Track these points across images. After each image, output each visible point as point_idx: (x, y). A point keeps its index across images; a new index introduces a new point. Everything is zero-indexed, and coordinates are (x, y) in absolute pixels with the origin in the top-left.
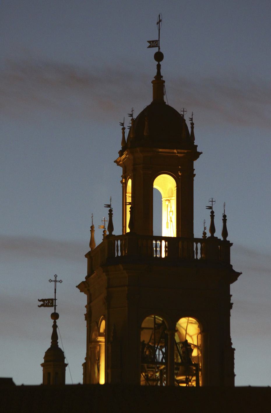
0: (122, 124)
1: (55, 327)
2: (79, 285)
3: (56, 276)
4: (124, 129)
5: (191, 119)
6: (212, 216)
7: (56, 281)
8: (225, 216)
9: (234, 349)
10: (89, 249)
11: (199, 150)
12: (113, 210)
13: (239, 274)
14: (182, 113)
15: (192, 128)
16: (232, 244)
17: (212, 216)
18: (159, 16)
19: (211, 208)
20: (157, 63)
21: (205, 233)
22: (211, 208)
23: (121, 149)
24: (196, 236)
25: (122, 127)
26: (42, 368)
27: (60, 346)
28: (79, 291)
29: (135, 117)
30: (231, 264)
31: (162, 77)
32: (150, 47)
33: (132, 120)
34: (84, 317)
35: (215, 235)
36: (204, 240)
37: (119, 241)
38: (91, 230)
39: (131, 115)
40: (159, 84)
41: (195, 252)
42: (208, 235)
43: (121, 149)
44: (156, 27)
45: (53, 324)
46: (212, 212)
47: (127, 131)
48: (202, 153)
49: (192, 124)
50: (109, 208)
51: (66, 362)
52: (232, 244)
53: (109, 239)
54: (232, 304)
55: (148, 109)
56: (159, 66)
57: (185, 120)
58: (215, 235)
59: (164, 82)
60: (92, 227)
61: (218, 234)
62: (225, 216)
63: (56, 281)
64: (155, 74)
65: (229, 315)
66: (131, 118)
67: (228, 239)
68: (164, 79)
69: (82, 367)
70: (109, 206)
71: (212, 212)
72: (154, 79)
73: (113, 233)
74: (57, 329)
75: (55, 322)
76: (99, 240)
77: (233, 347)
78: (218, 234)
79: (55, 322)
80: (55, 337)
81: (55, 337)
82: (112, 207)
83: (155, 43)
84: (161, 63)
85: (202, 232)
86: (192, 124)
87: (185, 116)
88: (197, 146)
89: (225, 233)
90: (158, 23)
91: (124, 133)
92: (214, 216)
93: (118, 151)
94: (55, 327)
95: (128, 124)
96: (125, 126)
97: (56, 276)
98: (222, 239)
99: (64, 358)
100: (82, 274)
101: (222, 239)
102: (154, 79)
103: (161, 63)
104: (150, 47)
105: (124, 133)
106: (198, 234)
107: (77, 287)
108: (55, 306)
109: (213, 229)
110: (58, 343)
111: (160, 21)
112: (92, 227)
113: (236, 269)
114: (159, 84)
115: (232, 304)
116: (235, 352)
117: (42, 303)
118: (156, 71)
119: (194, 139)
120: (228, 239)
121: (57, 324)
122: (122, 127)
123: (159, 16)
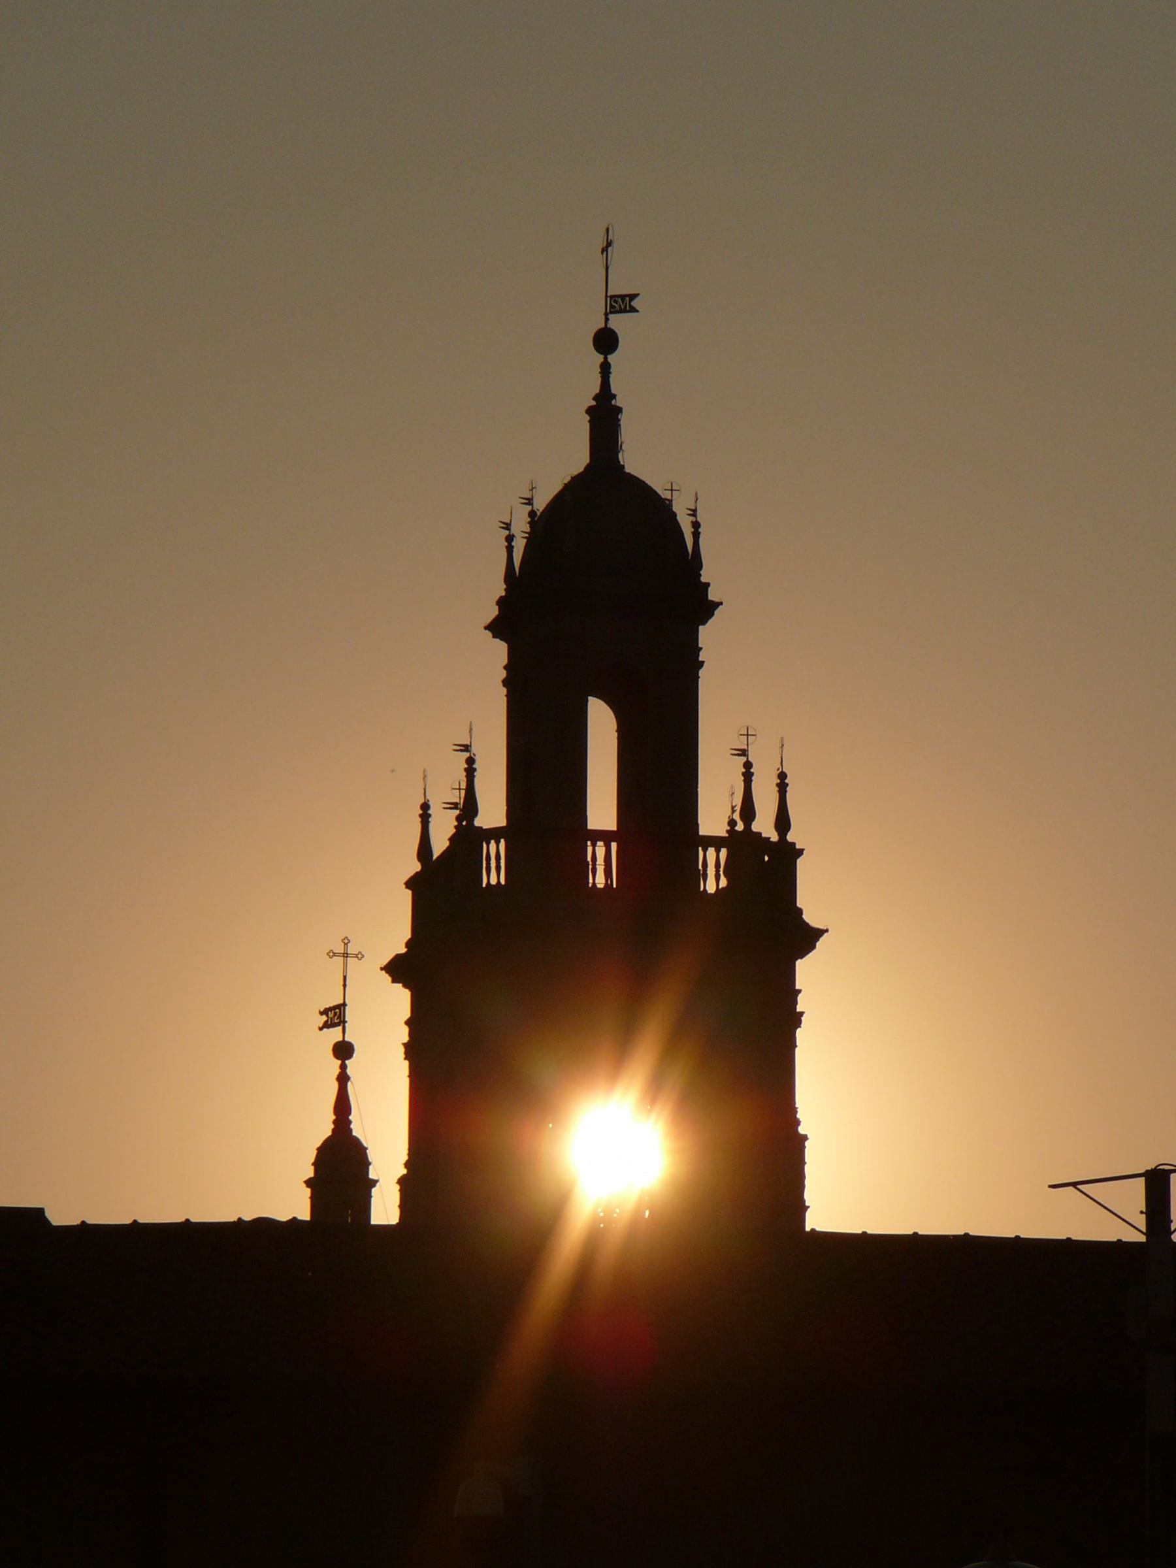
0: (507, 526)
1: (343, 1079)
2: (389, 963)
3: (346, 942)
4: (510, 539)
5: (694, 513)
6: (748, 776)
7: (346, 955)
8: (782, 776)
9: (805, 1138)
10: (417, 867)
11: (713, 595)
12: (477, 758)
13: (820, 933)
14: (666, 495)
15: (696, 535)
16: (801, 852)
17: (748, 776)
18: (608, 230)
19: (744, 753)
20: (601, 358)
21: (732, 823)
22: (744, 753)
23: (503, 594)
24: (591, 825)
25: (507, 532)
26: (308, 1192)
27: (357, 1130)
28: (390, 979)
29: (540, 505)
30: (799, 905)
31: (614, 396)
32: (633, 297)
33: (532, 514)
34: (403, 1050)
35: (755, 827)
36: (740, 842)
37: (502, 840)
38: (421, 816)
39: (529, 501)
40: (604, 417)
41: (721, 869)
42: (740, 827)
43: (503, 594)
44: (600, 259)
45: (338, 1071)
46: (748, 765)
47: (519, 545)
48: (721, 603)
49: (696, 525)
50: (467, 755)
51: (372, 1175)
52: (801, 852)
53: (468, 837)
54: (802, 1014)
55: (574, 487)
56: (605, 369)
57: (675, 515)
58: (755, 827)
59: (620, 410)
60: (425, 807)
61: (765, 826)
62: (782, 776)
63: (346, 955)
64: (596, 390)
65: (793, 1045)
66: (529, 508)
67: (790, 838)
68: (618, 402)
69: (398, 1187)
70: (466, 748)
71: (748, 765)
72: (594, 403)
73: (478, 822)
74: (349, 1084)
75: (343, 1067)
76: (439, 845)
77: (802, 1130)
78: (765, 826)
79: (343, 1067)
80: (342, 1107)
81: (342, 1107)
82: (474, 749)
83: (616, 302)
84: (610, 358)
85: (727, 820)
86: (696, 525)
87: (674, 503)
88: (708, 585)
89: (783, 822)
90: (604, 250)
91: (510, 549)
92: (752, 774)
93: (497, 598)
94: (343, 1079)
95: (521, 527)
96: (513, 531)
97: (346, 942)
98: (775, 838)
99: (368, 1164)
100: (396, 934)
101: (775, 838)
102: (594, 403)
103: (610, 358)
104: (633, 297)
105: (510, 549)
106: (713, 819)
107: (382, 969)
108: (345, 1022)
109: (748, 810)
110: (350, 1122)
111: (609, 244)
112: (425, 807)
113: (811, 917)
114: (604, 417)
115: (802, 1014)
116: (807, 1143)
117: (324, 1018)
118: (599, 380)
119: (701, 567)
120: (790, 838)
121: (349, 1071)
122: (507, 532)
123: (608, 230)
